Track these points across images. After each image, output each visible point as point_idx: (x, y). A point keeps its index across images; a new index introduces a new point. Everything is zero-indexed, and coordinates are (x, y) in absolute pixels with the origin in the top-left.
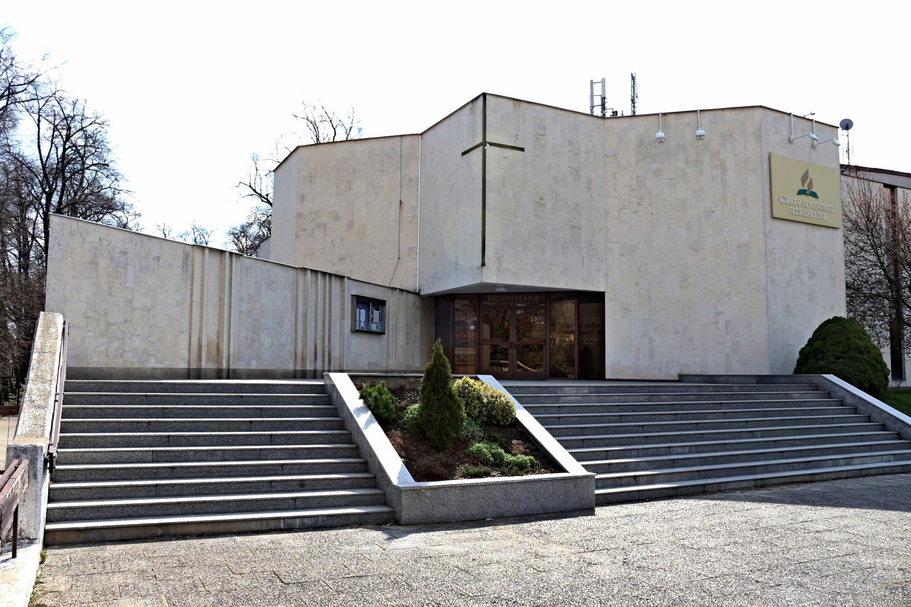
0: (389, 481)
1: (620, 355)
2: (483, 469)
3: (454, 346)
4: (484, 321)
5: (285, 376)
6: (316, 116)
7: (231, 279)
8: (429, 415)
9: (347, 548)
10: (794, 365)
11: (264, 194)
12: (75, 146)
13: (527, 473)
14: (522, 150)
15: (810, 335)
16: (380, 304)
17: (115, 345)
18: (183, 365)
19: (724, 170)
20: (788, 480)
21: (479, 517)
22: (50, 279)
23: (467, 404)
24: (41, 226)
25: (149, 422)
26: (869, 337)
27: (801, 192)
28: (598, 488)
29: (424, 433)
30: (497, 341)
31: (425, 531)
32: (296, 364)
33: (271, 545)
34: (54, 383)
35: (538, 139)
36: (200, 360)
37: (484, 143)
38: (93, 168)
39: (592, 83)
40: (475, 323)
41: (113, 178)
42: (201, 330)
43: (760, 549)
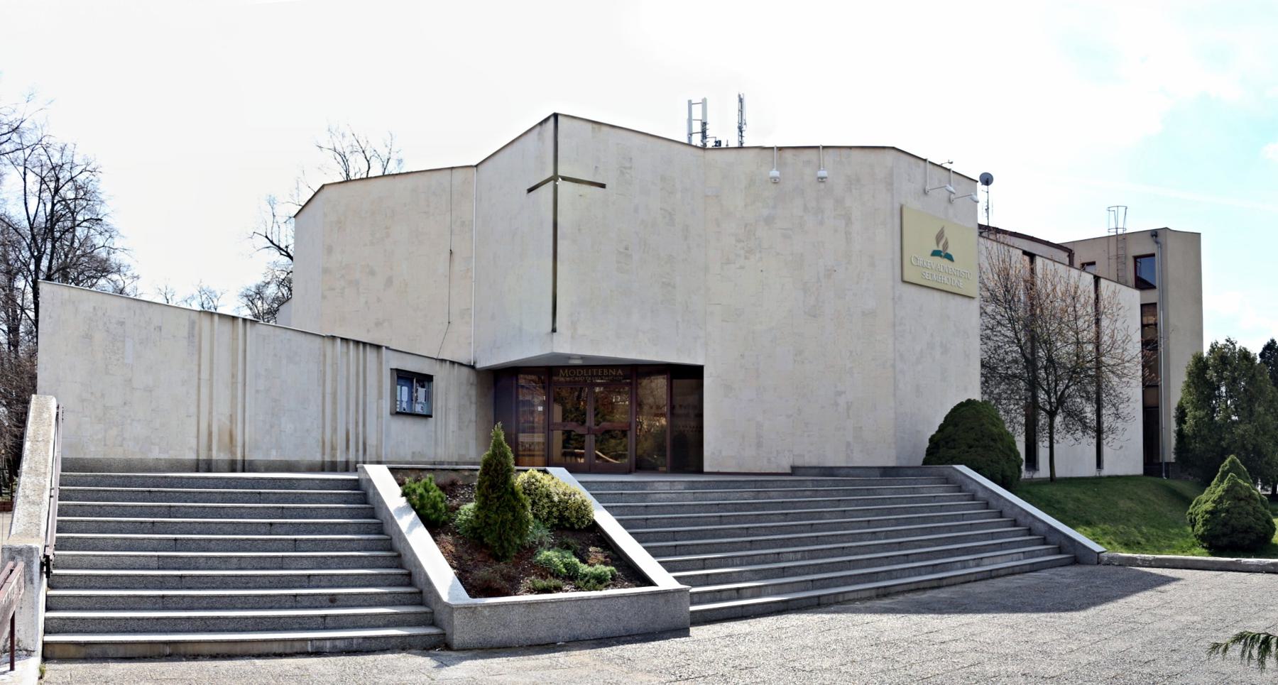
0: (438, 597)
2: (553, 582)
3: (518, 431)
4: (555, 400)
5: (311, 469)
6: (343, 145)
7: (245, 351)
8: (487, 516)
9: (388, 676)
10: (923, 454)
11: (282, 246)
12: (64, 200)
13: (607, 587)
14: (603, 186)
15: (940, 420)
16: (425, 380)
17: (114, 432)
18: (190, 456)
19: (848, 220)
20: (913, 587)
21: (548, 640)
22: (42, 357)
23: (534, 503)
24: (30, 296)
25: (153, 523)
26: (1003, 422)
27: (935, 253)
28: (693, 604)
29: (481, 538)
30: (571, 426)
31: (482, 658)
32: (323, 454)
33: (297, 671)
34: (49, 476)
35: (622, 173)
36: (210, 449)
37: (555, 178)
38: (85, 224)
39: (690, 104)
40: (544, 404)
41: (107, 235)
42: (210, 413)
43: (881, 667)
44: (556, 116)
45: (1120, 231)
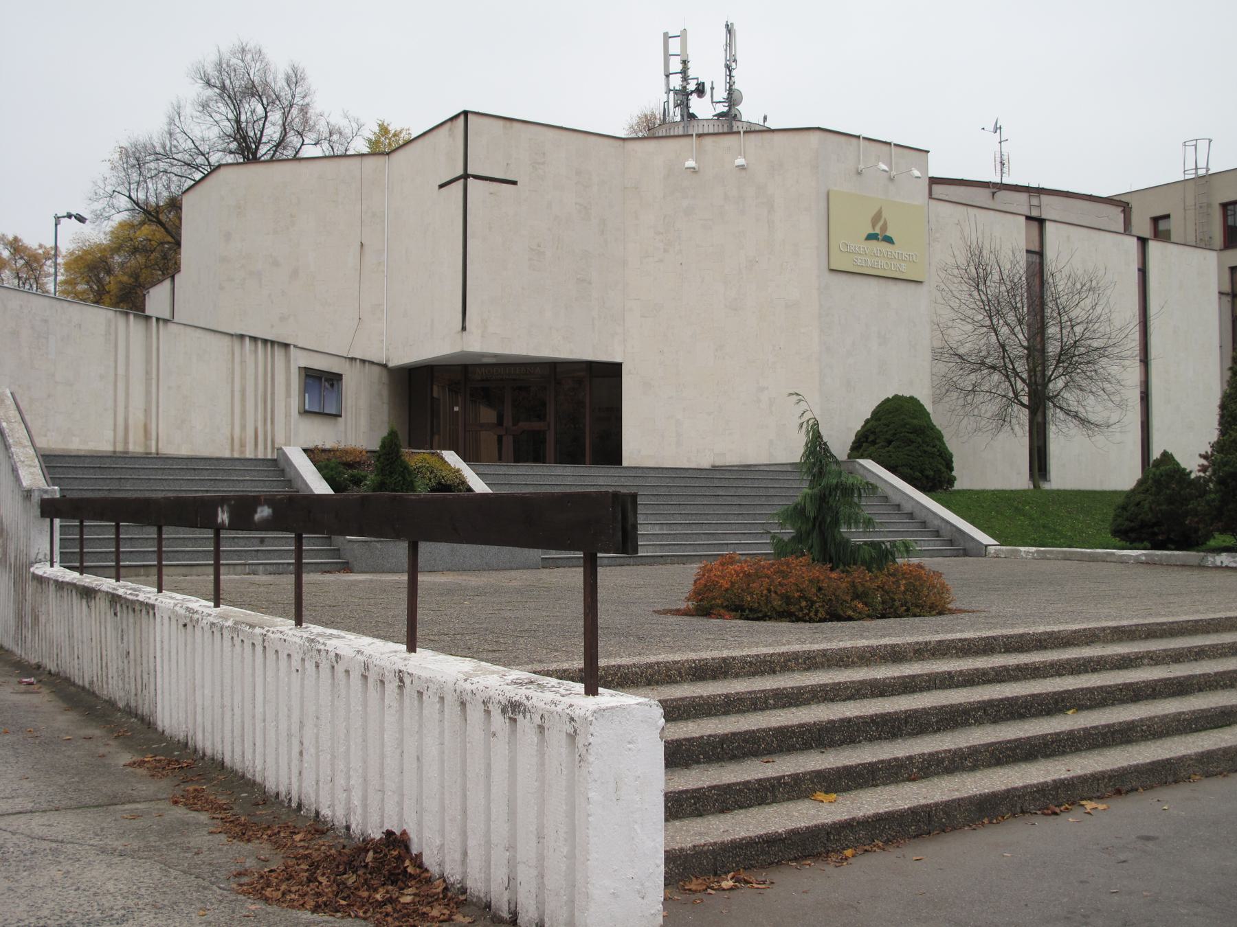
1: (653, 435)
14: (515, 183)
16: (332, 380)
27: (871, 237)
32: (232, 450)
37: (466, 176)
39: (667, 37)
42: (126, 407)
44: (466, 113)
45: (1202, 172)
